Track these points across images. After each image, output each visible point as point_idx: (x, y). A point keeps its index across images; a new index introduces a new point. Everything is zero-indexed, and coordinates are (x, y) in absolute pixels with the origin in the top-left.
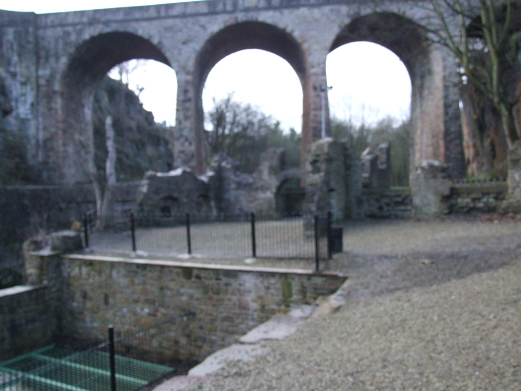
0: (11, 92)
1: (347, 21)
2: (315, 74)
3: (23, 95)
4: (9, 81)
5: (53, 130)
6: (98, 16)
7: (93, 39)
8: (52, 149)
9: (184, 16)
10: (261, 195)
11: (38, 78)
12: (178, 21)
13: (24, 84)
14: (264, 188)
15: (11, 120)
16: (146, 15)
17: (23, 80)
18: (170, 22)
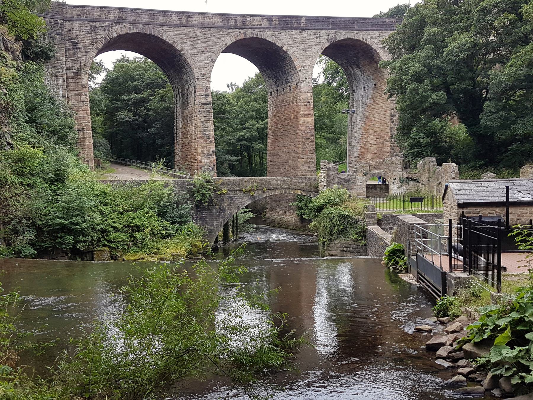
6: (124, 15)
9: (202, 26)
12: (198, 31)
16: (169, 21)
18: (191, 30)
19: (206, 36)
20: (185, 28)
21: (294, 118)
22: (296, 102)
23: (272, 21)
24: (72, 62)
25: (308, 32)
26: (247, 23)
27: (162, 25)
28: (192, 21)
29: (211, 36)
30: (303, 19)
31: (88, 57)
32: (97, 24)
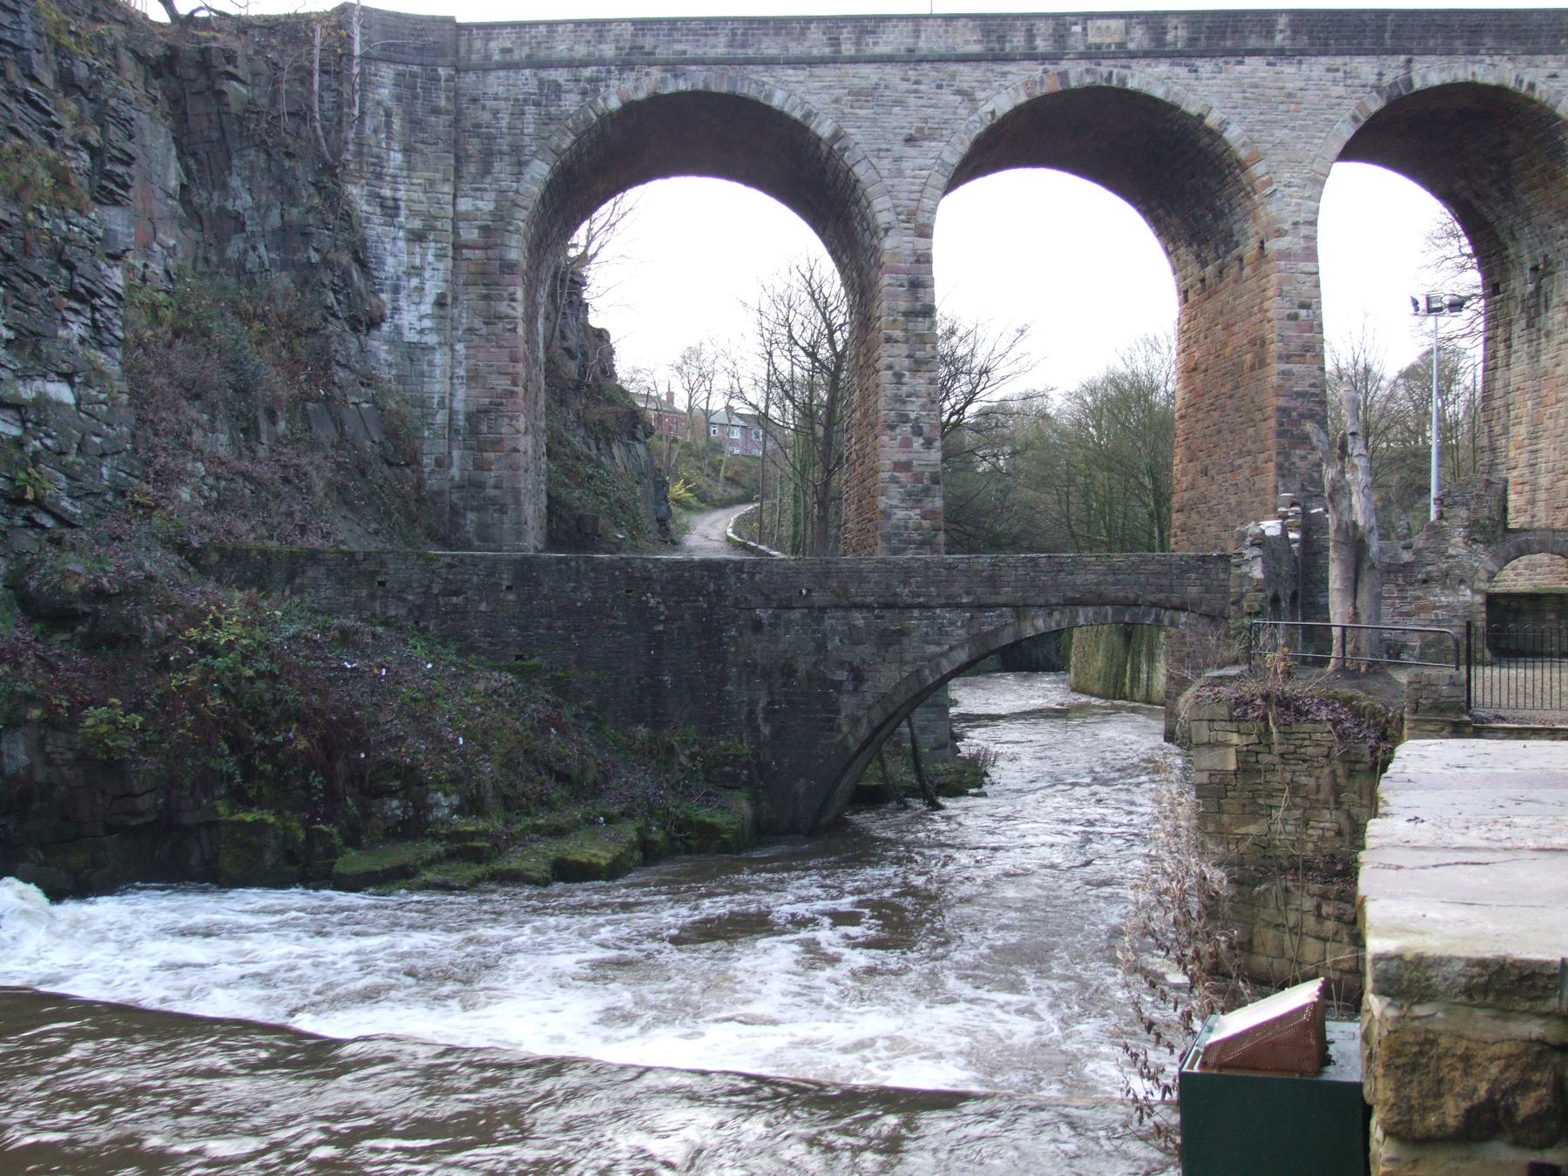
0: (381, 262)
1: (1375, 104)
2: (1285, 255)
3: (416, 271)
4: (376, 228)
5: (503, 383)
6: (648, 42)
7: (630, 108)
8: (496, 444)
9: (911, 58)
10: (1440, 597)
11: (457, 218)
12: (892, 73)
13: (417, 237)
14: (1448, 580)
15: (379, 346)
16: (796, 50)
17: (417, 224)
18: (870, 73)
19: (922, 87)
20: (850, 69)
21: (1252, 368)
22: (1260, 310)
23: (1164, 31)
24: (475, 198)
25: (1300, 62)
26: (1071, 41)
27: (768, 62)
28: (875, 44)
29: (940, 87)
30: (1282, 22)
31: (527, 177)
32: (561, 75)
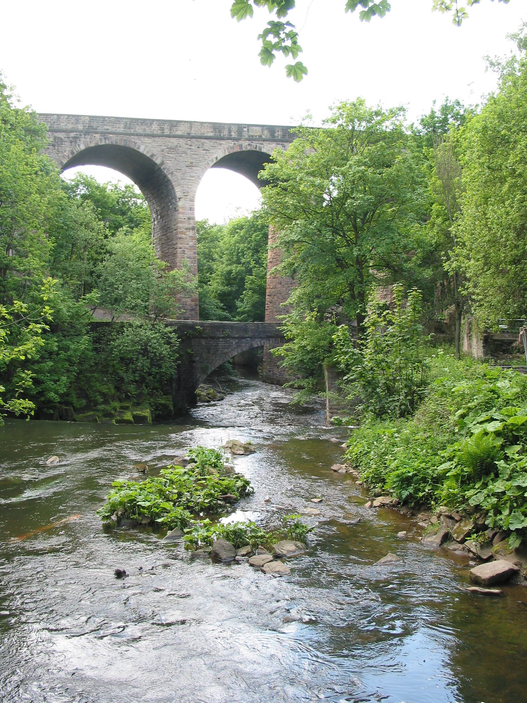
9: (189, 137)
12: (182, 141)
